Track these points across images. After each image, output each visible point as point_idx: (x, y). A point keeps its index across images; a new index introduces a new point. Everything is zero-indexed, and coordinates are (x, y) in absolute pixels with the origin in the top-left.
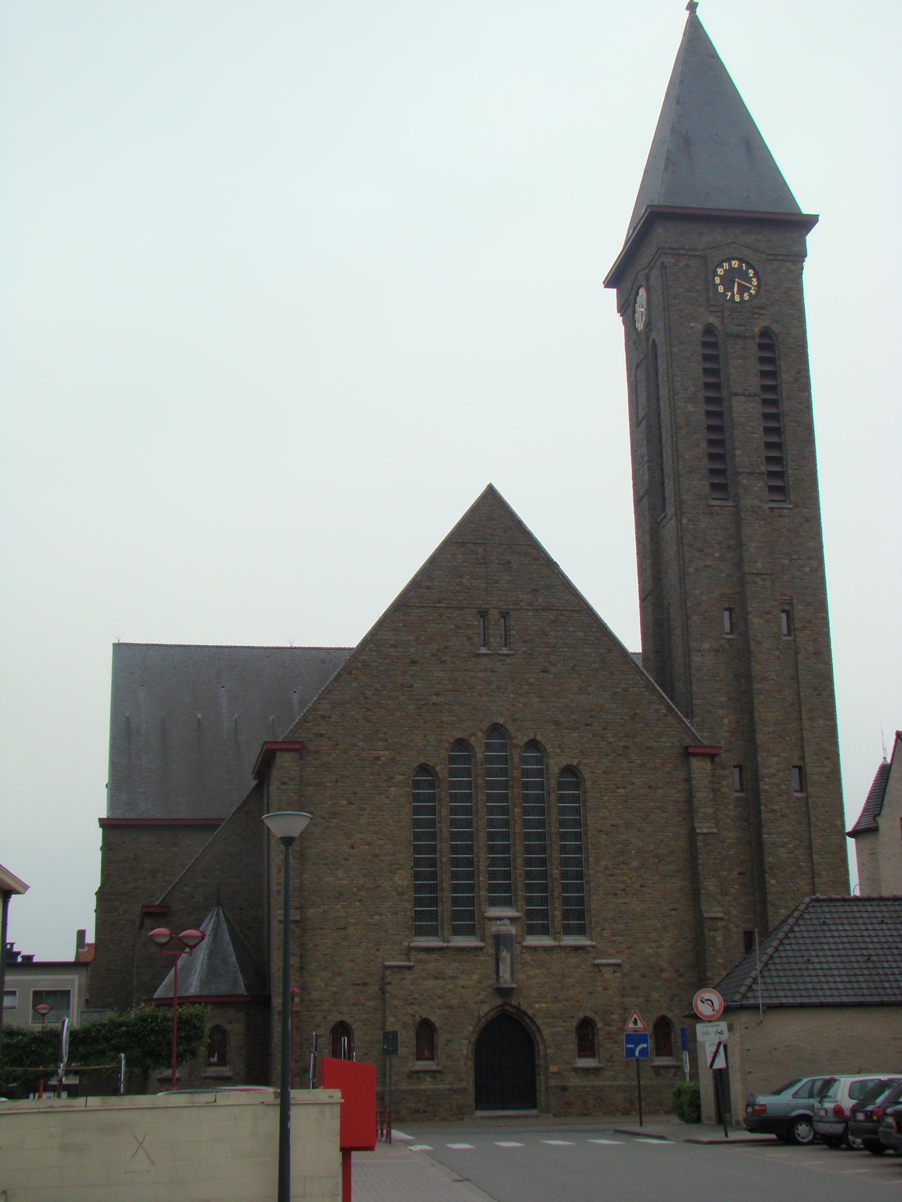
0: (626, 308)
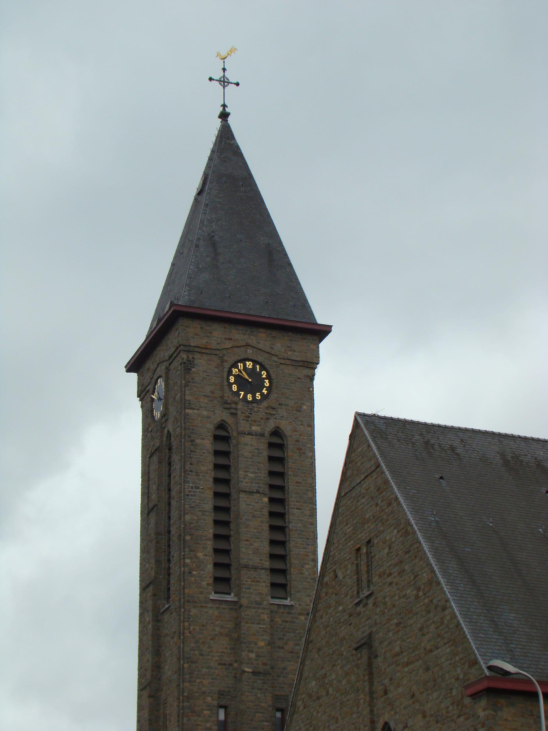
0: (144, 393)
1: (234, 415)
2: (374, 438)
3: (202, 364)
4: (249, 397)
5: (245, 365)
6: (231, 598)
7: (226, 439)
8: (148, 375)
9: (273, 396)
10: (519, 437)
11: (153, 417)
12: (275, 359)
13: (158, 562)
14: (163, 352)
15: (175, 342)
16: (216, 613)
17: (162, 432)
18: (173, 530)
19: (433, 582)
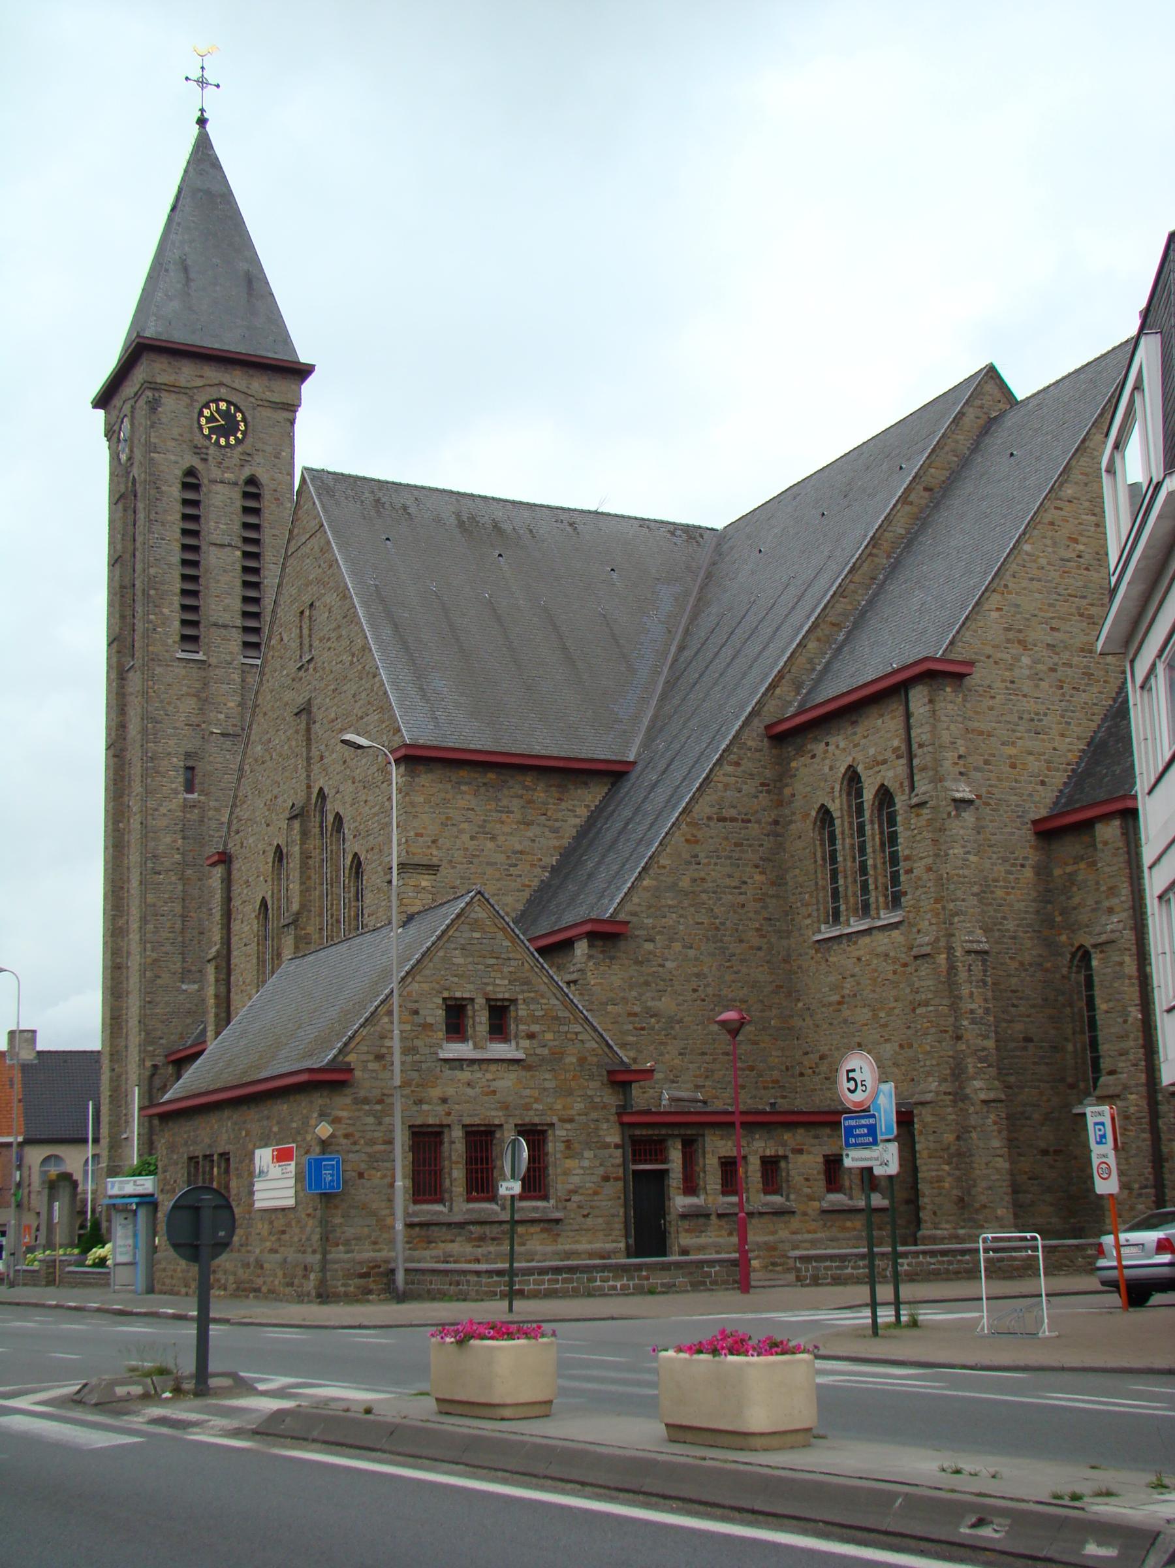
1: (205, 460)
2: (319, 495)
3: (169, 403)
4: (223, 441)
5: (218, 406)
6: (200, 656)
7: (196, 487)
8: (115, 413)
9: (249, 440)
10: (479, 496)
11: (119, 460)
12: (252, 399)
13: (123, 617)
14: (129, 389)
16: (183, 672)
17: (128, 477)
18: (138, 584)
19: (366, 648)
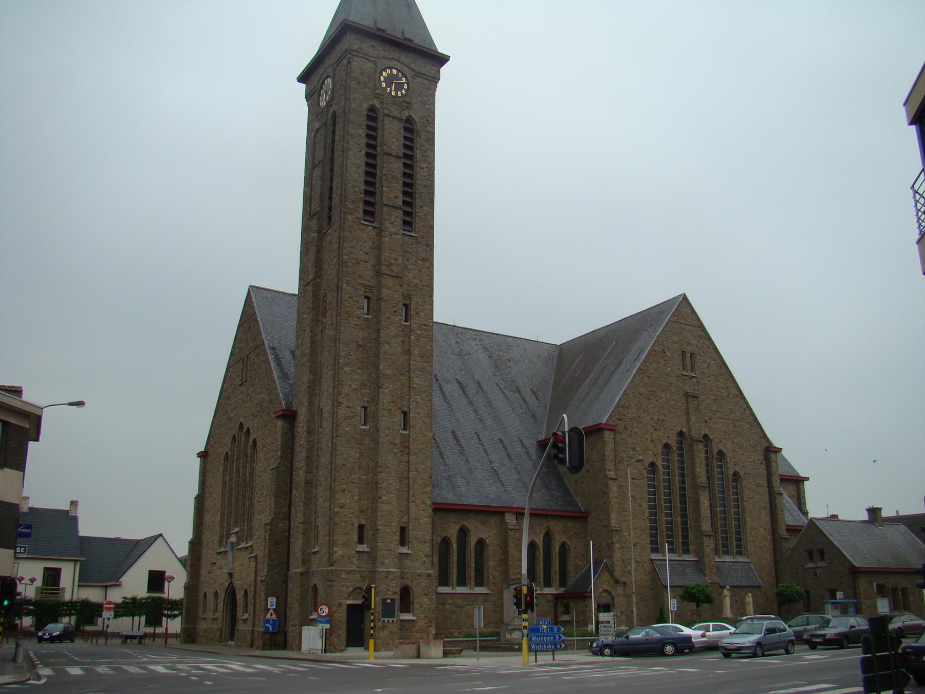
15: (344, 48)
